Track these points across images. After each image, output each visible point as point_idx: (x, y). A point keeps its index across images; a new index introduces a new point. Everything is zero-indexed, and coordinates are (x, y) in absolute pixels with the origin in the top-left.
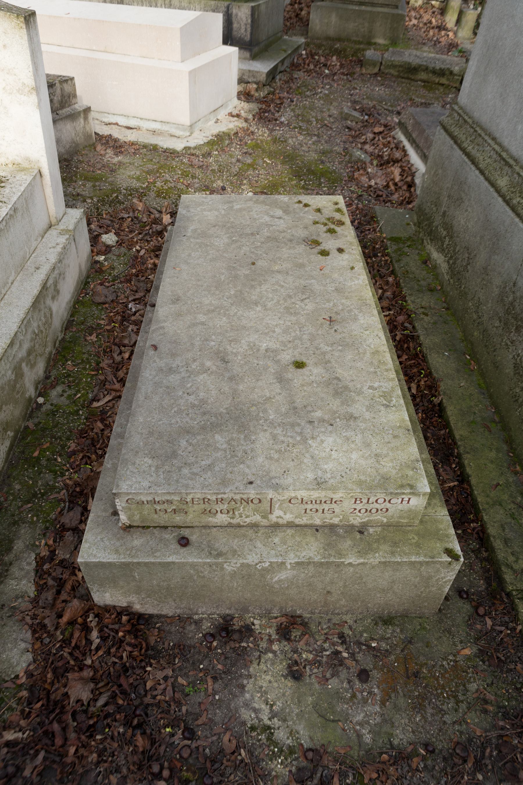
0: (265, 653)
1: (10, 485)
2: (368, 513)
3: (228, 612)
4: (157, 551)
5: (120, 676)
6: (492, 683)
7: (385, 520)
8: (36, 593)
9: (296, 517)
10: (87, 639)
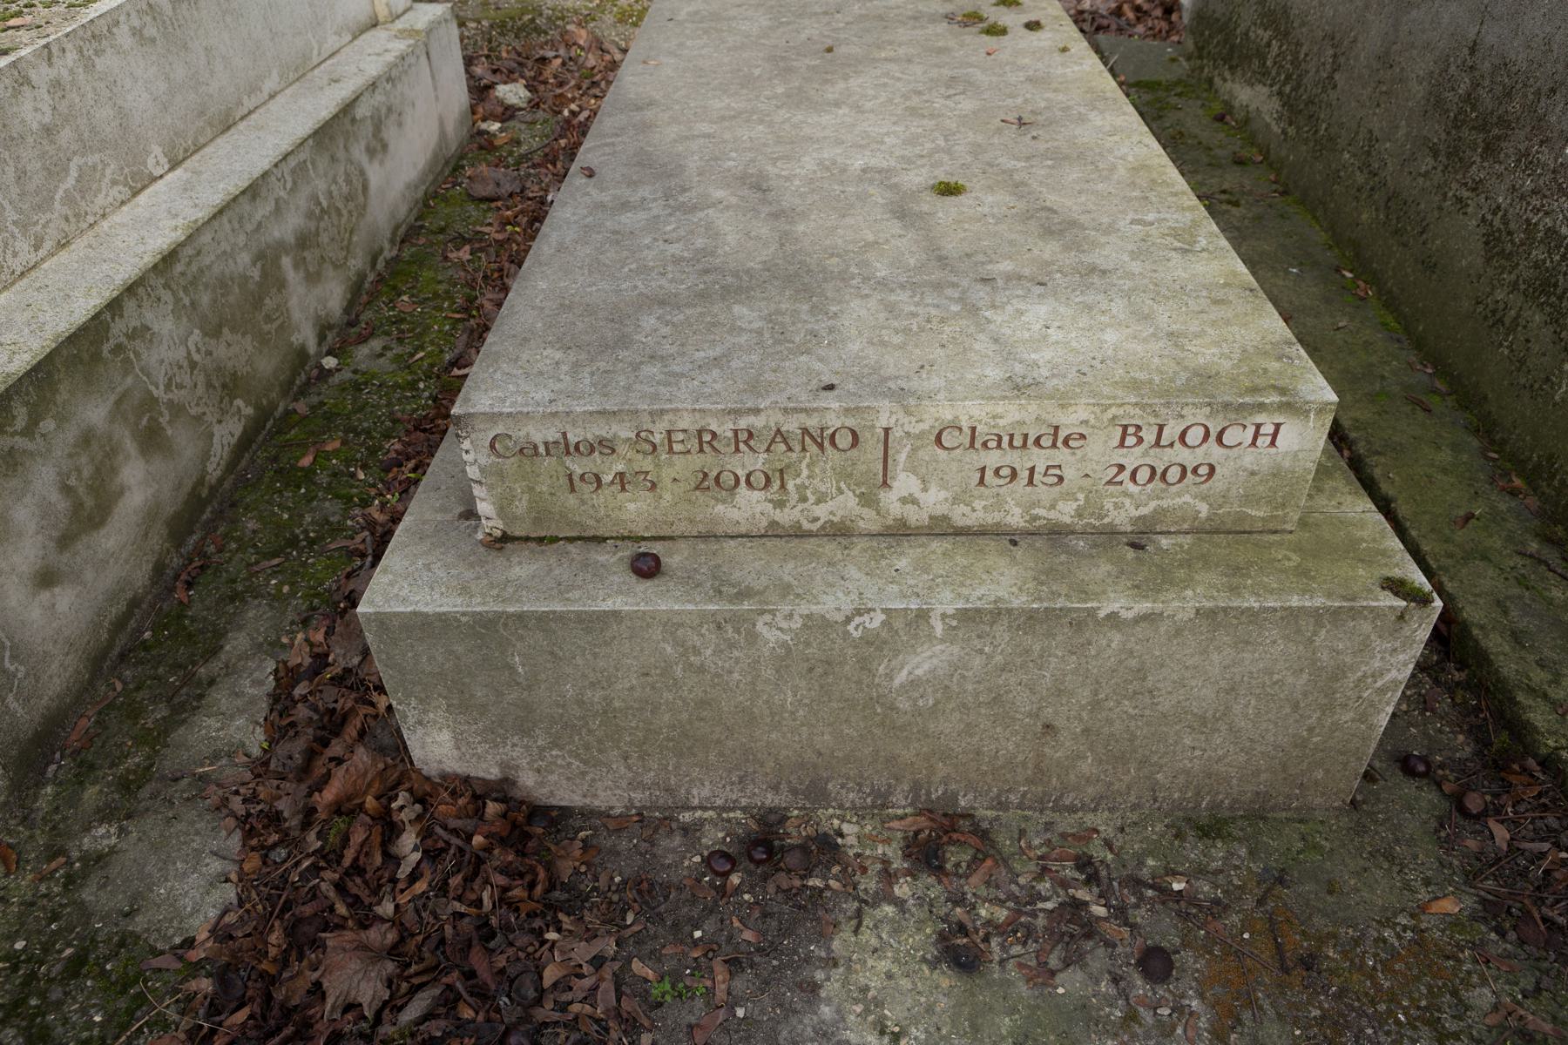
0: (875, 904)
1: (234, 521)
2: (1157, 483)
3: (771, 799)
4: (572, 588)
5: (470, 946)
6: (1538, 990)
7: (1204, 509)
8: (265, 745)
9: (956, 500)
10: (387, 855)
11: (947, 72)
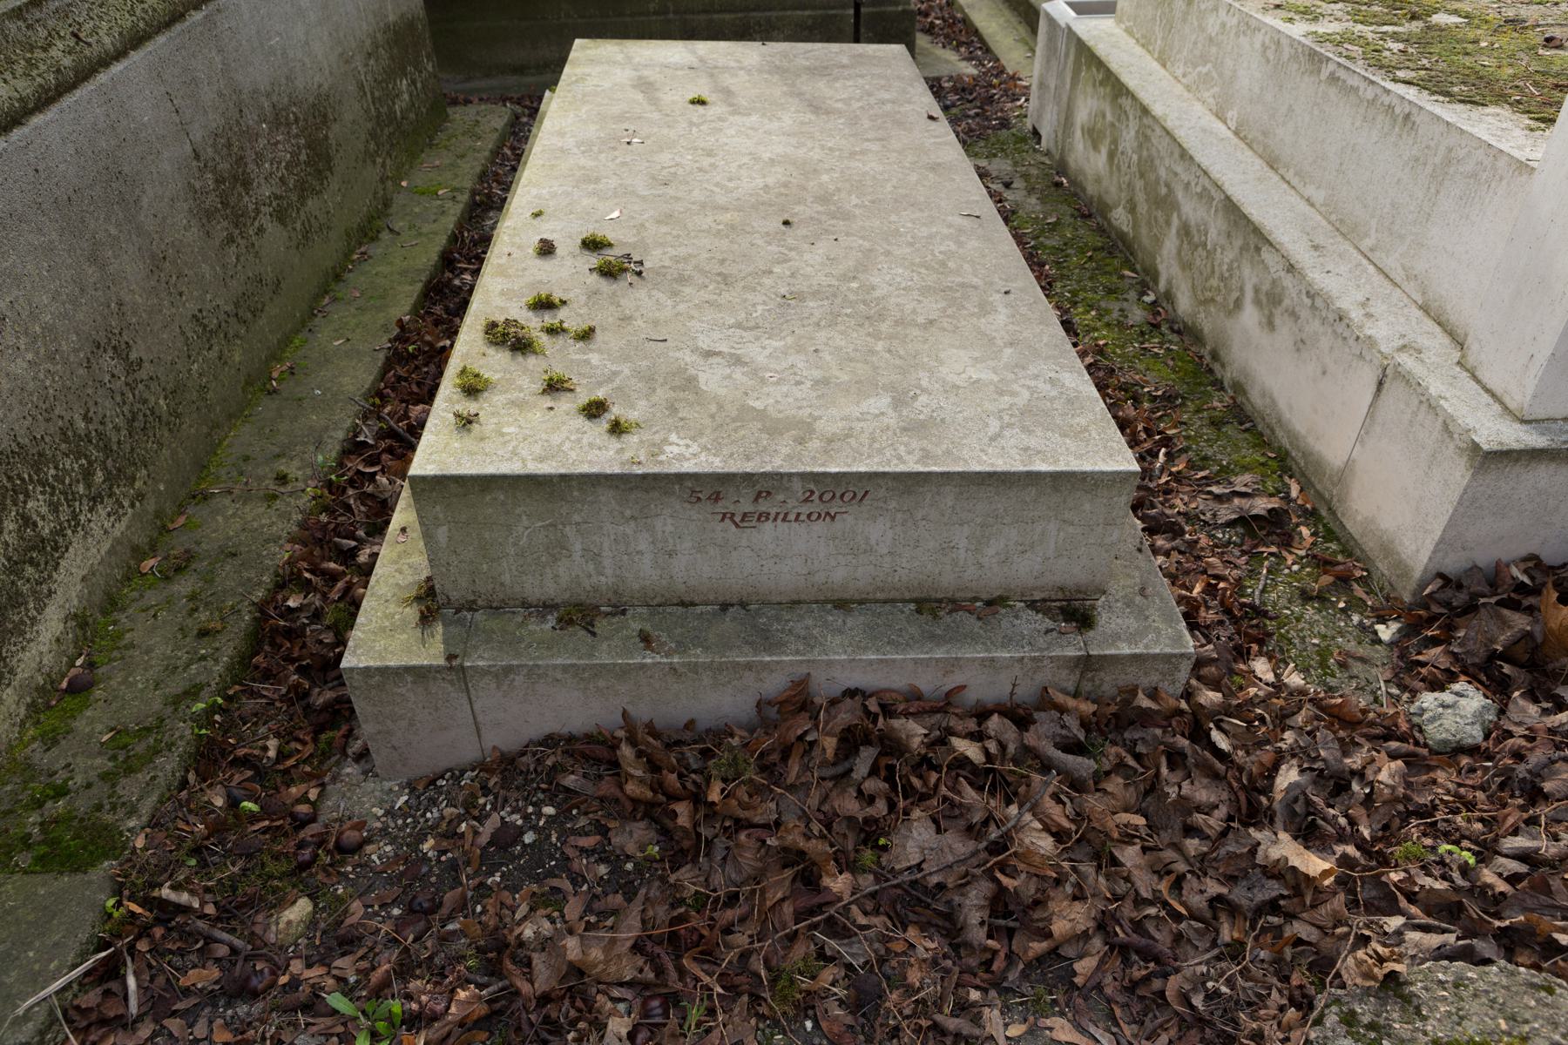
11: (670, 191)
